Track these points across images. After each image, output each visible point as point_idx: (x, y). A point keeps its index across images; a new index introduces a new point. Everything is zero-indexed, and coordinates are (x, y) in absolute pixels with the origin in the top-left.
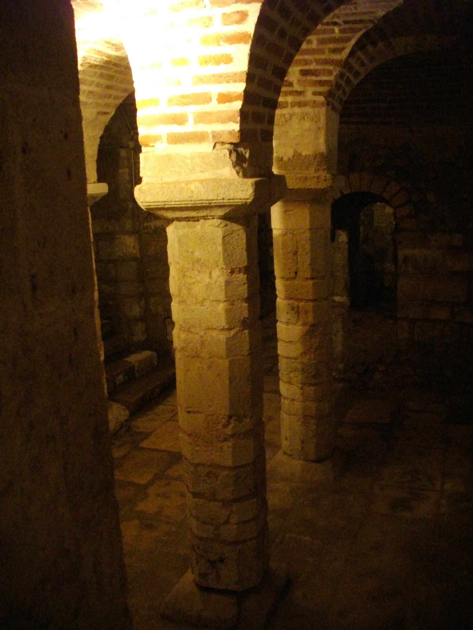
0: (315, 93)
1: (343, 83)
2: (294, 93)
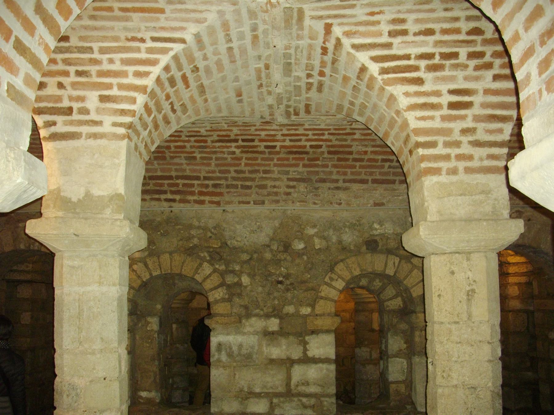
0: (115, 124)
1: (149, 120)
2: (90, 123)
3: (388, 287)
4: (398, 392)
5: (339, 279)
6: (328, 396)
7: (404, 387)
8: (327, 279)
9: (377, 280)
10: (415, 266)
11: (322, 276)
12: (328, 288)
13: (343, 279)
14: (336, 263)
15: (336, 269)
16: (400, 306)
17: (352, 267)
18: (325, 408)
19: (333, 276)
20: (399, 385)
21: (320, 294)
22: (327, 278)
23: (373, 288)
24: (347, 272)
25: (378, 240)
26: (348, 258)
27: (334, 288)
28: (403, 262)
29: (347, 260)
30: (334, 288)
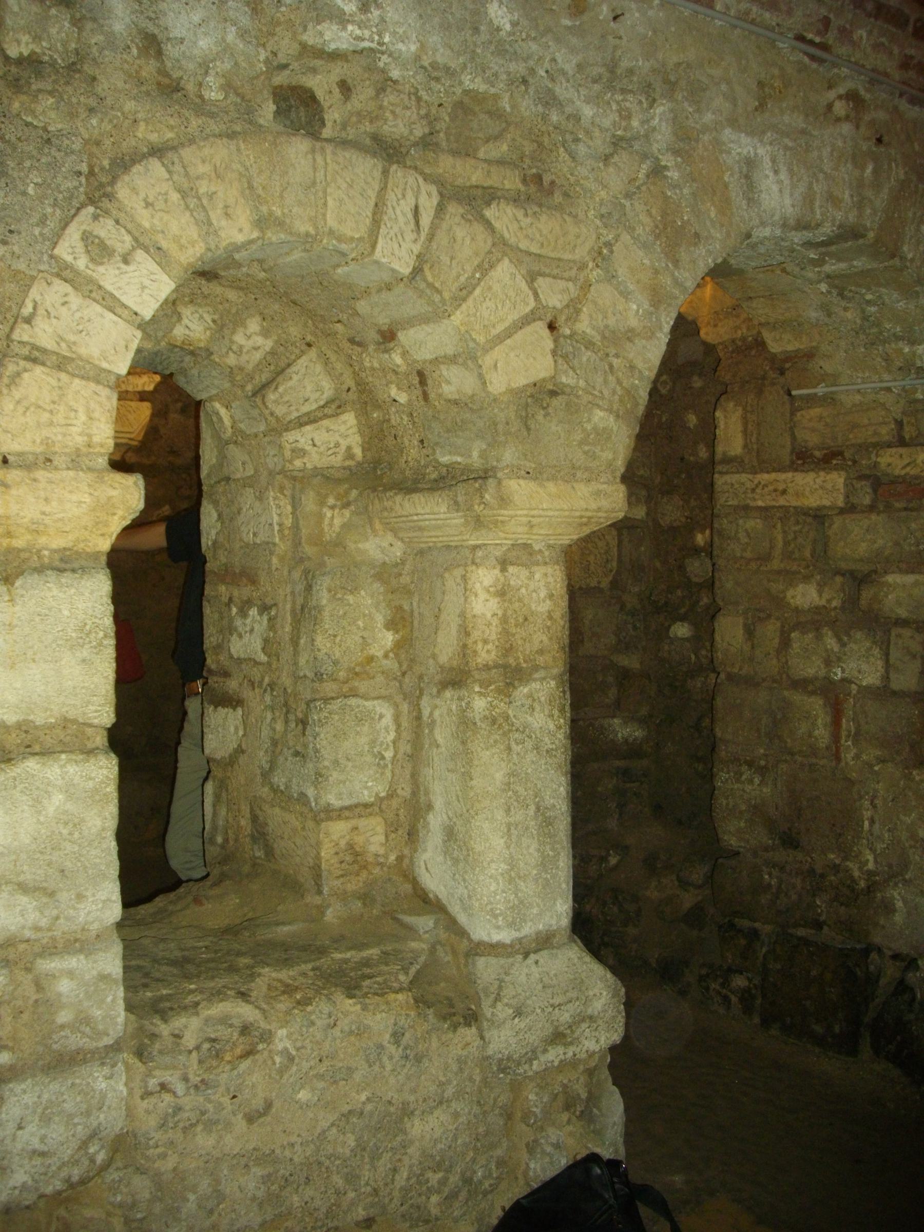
3: (303, 361)
4: (355, 856)
5: (140, 255)
6: (77, 944)
7: (380, 829)
8: (70, 249)
9: (254, 325)
10: (505, 243)
11: (43, 222)
12: (75, 300)
13: (160, 254)
14: (123, 164)
15: (122, 191)
16: (349, 455)
17: (211, 196)
18: (64, 1017)
19: (106, 230)
20: (362, 823)
21: (22, 333)
22: (73, 234)
23: (232, 360)
24: (186, 217)
25: (320, 94)
26: (192, 141)
27: (111, 303)
28: (454, 209)
29: (187, 153)
30: (111, 303)
